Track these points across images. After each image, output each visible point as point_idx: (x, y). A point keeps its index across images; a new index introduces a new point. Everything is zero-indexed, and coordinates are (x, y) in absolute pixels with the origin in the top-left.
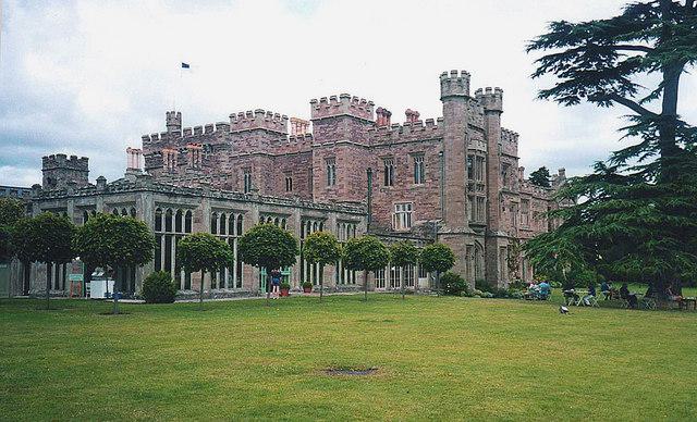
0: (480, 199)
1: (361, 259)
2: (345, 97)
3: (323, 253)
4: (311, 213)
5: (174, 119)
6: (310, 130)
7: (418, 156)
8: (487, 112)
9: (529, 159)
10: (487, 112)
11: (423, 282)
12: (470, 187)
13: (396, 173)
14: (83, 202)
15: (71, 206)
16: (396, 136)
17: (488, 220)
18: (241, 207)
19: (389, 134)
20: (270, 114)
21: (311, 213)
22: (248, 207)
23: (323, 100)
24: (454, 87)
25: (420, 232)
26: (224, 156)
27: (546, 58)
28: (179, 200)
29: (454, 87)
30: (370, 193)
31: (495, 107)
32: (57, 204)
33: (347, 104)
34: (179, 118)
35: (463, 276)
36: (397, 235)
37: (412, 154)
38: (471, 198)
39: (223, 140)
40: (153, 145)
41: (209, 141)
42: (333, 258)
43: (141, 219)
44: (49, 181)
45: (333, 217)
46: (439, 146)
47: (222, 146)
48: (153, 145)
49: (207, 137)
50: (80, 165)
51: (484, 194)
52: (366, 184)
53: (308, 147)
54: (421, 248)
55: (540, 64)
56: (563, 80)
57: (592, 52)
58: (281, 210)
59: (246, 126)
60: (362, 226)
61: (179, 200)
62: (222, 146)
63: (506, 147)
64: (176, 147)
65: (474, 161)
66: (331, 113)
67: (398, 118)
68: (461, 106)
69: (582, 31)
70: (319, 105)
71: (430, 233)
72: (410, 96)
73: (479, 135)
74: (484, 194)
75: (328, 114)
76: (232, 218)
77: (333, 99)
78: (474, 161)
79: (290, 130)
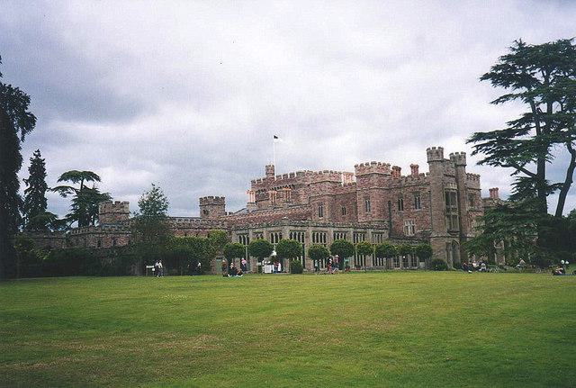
0: (455, 217)
1: (383, 253)
2: (373, 163)
3: (365, 250)
4: (359, 230)
5: (270, 170)
6: (355, 180)
7: (416, 194)
8: (457, 166)
9: (485, 187)
10: (457, 166)
11: (422, 264)
12: (448, 210)
13: (404, 204)
14: (257, 231)
15: (251, 232)
16: (403, 182)
17: (460, 229)
18: (325, 229)
19: (400, 182)
20: (331, 172)
21: (359, 230)
22: (328, 229)
23: (362, 165)
24: (435, 155)
25: (420, 237)
26: (301, 191)
27: (477, 146)
28: (299, 229)
29: (435, 155)
30: (390, 215)
31: (461, 163)
32: (244, 232)
33: (375, 166)
34: (273, 169)
35: (445, 261)
36: (406, 238)
37: (413, 193)
38: (448, 216)
39: (299, 182)
40: (257, 185)
41: (292, 183)
42: (370, 253)
43: (265, 239)
44: (205, 212)
45: (370, 231)
46: (428, 188)
47: (301, 185)
48: (257, 185)
49: (291, 180)
50: (219, 202)
51: (457, 214)
52: (387, 210)
53: (354, 190)
54: (416, 245)
55: (475, 149)
56: (489, 156)
57: (501, 142)
58: (344, 230)
59: (319, 180)
60: (386, 235)
61: (299, 229)
62: (301, 185)
63: (471, 184)
64: (268, 186)
65: (448, 196)
66: (366, 172)
67: (406, 172)
68: (440, 166)
69: (491, 135)
70: (359, 168)
71: (425, 237)
72: (410, 158)
73: (453, 179)
74: (457, 214)
75: (364, 172)
76: (295, 234)
77: (367, 164)
78: (448, 196)
79: (343, 180)
